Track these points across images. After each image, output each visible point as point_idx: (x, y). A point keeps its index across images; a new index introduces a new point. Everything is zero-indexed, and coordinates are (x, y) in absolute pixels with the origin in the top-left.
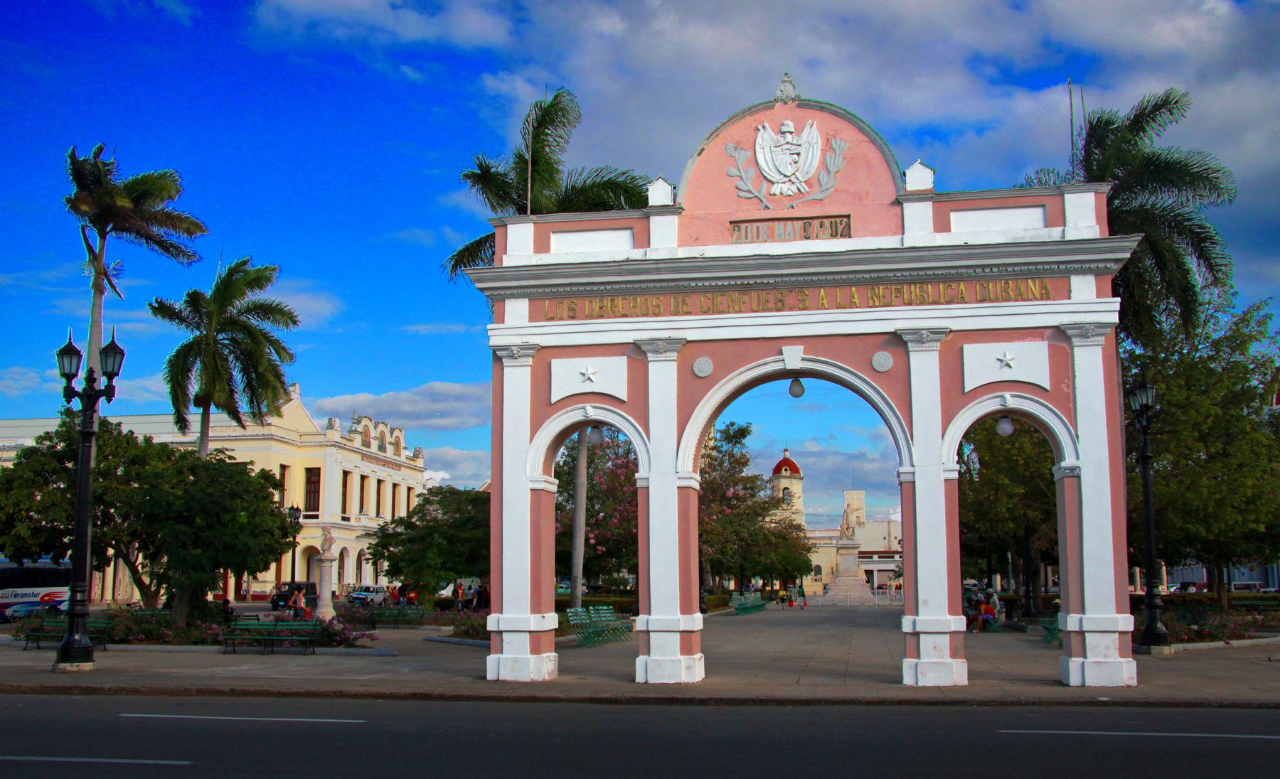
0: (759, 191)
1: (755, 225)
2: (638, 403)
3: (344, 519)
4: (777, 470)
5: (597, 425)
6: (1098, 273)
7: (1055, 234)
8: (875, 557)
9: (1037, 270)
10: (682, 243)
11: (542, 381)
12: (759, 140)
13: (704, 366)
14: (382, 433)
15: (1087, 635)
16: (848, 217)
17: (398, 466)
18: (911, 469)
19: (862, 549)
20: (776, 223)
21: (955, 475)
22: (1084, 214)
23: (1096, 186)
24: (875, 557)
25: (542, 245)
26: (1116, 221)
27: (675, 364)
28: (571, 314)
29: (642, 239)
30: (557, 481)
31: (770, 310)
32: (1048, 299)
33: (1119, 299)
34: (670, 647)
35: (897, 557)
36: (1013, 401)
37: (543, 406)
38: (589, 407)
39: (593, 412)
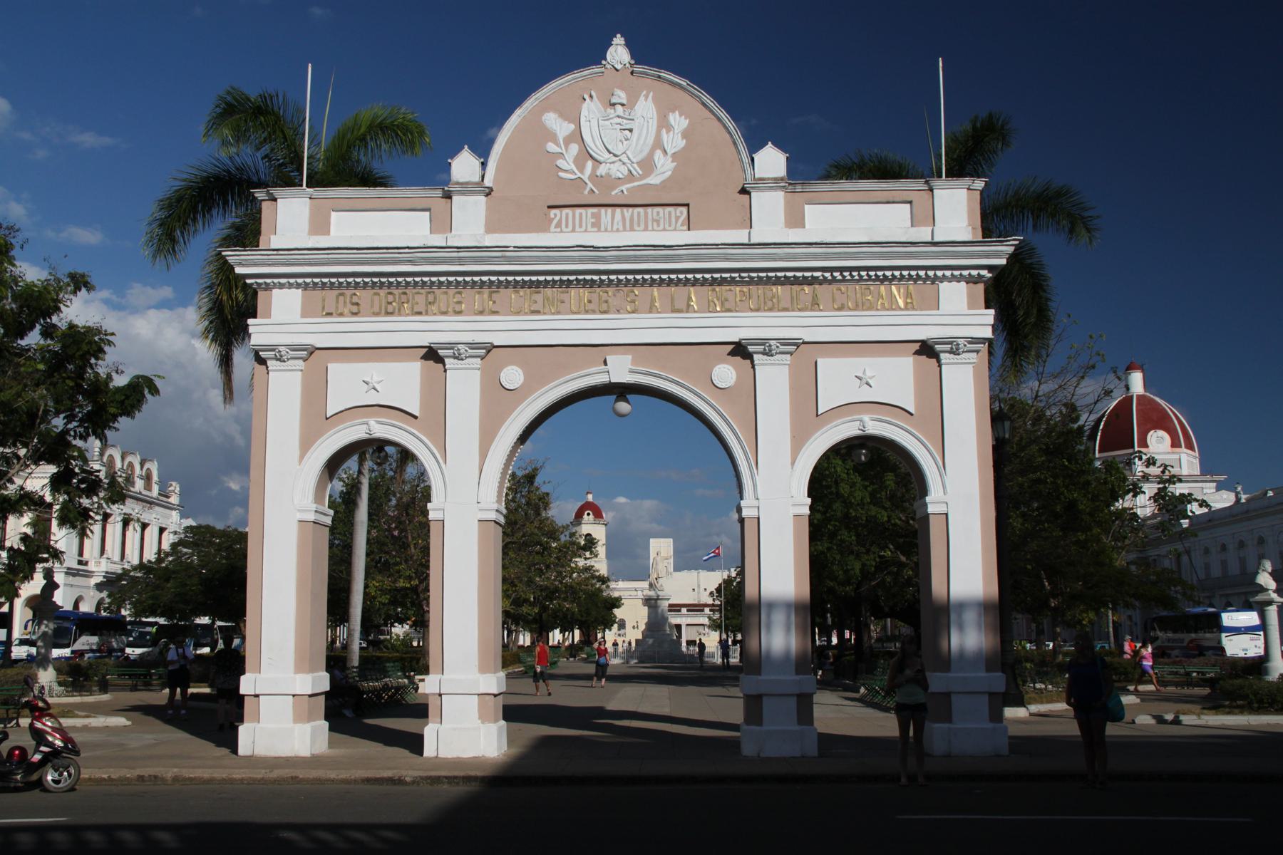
0: (582, 171)
1: (578, 211)
2: (434, 417)
3: (80, 563)
4: (579, 515)
5: (378, 445)
6: (971, 280)
7: (923, 234)
8: (684, 610)
9: (911, 273)
10: (490, 228)
11: (315, 391)
12: (584, 113)
13: (513, 376)
14: (131, 465)
15: (954, 698)
16: (688, 205)
17: (151, 503)
18: (756, 503)
19: (671, 602)
20: (603, 210)
21: (807, 511)
22: (955, 207)
23: (967, 181)
24: (684, 610)
25: (320, 225)
26: (994, 219)
27: (478, 372)
28: (355, 309)
29: (442, 223)
30: (331, 512)
31: (594, 312)
32: (913, 309)
33: (992, 312)
34: (465, 724)
35: (707, 610)
36: (875, 427)
37: (316, 417)
38: (372, 422)
39: (380, 430)
